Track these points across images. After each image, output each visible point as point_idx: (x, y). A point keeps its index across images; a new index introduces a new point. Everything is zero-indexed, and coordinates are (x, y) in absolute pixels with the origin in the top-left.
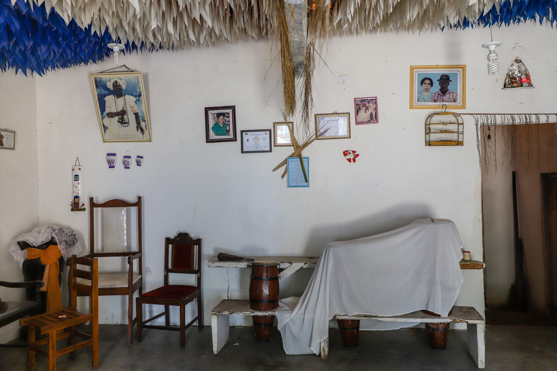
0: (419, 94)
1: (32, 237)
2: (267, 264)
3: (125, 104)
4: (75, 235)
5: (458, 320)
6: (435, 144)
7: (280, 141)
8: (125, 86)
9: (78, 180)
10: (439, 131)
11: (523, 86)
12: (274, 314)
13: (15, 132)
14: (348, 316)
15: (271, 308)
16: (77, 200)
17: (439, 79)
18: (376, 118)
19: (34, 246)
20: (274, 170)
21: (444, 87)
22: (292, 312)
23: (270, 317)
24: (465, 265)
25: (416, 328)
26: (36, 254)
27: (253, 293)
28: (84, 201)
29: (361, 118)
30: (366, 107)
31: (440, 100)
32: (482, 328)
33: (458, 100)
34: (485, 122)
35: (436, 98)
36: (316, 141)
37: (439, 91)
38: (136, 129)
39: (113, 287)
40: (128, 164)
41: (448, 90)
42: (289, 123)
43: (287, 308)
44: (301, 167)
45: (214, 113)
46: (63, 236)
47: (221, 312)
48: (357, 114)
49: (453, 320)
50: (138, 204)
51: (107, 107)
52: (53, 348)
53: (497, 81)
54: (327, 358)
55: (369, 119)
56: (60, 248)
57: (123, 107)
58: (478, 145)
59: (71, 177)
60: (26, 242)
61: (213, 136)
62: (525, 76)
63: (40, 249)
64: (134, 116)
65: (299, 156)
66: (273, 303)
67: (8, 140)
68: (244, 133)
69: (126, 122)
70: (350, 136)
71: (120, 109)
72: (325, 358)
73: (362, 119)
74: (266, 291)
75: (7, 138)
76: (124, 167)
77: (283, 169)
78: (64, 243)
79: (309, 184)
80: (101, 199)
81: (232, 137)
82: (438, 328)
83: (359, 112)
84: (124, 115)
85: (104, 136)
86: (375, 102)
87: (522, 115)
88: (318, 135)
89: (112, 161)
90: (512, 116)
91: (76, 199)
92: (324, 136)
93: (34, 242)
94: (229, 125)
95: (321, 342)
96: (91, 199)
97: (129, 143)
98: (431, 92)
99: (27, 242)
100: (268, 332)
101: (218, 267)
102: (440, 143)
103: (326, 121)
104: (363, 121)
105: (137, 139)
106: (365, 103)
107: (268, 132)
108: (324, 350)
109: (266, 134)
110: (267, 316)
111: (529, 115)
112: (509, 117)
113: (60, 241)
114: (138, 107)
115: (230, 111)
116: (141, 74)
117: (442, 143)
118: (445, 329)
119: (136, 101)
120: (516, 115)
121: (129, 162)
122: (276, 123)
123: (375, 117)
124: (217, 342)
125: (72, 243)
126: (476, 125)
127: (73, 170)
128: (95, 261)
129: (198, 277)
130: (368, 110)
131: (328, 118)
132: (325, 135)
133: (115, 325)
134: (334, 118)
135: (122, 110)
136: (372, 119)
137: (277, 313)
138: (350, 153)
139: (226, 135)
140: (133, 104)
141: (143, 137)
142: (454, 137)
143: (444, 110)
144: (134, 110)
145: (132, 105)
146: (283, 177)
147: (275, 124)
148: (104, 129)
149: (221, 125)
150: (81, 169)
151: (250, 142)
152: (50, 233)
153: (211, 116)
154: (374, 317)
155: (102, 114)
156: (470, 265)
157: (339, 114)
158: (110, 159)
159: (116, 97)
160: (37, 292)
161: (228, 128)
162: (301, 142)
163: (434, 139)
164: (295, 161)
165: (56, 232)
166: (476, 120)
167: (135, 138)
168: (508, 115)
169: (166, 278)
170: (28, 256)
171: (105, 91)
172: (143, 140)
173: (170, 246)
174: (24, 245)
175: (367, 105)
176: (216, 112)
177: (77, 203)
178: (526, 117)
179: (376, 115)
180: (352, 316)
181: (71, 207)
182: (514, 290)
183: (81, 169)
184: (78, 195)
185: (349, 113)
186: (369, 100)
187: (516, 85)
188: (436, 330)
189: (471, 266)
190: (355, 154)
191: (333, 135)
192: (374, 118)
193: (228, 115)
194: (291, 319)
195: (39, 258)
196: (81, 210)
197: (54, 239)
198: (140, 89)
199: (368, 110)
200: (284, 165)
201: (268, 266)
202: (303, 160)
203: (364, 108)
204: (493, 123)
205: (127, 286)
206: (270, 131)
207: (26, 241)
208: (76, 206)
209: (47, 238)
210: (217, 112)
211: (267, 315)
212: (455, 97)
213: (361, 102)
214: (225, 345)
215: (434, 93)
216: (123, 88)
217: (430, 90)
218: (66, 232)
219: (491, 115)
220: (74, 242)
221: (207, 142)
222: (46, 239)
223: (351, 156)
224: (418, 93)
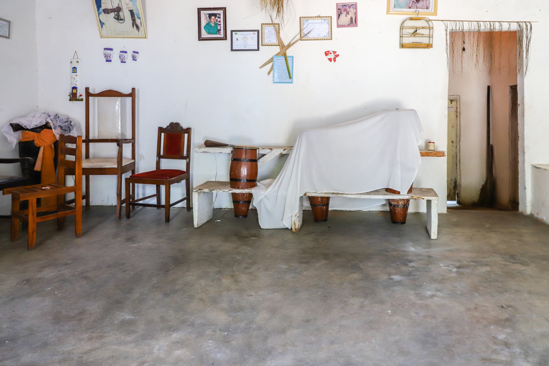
1: (27, 120)
2: (246, 147)
4: (71, 121)
5: (415, 196)
7: (266, 41)
9: (76, 72)
12: (251, 192)
14: (317, 193)
15: (249, 187)
16: (74, 91)
18: (355, 22)
19: (28, 129)
20: (261, 67)
22: (266, 190)
23: (248, 195)
24: (428, 153)
25: (386, 211)
26: (31, 136)
27: (233, 173)
28: (81, 92)
30: (347, 11)
31: (415, 7)
32: (435, 203)
33: (431, 7)
34: (454, 28)
35: (410, 5)
36: (300, 42)
38: (132, 25)
39: (103, 167)
40: (124, 58)
42: (276, 24)
43: (264, 187)
44: (286, 65)
45: (206, 14)
46: (58, 121)
47: (202, 189)
48: (339, 18)
49: (411, 197)
50: (132, 94)
51: (103, 3)
52: (33, 214)
54: (298, 231)
55: (350, 23)
56: (55, 132)
57: (119, 4)
58: (447, 49)
59: (70, 70)
60: (19, 124)
61: (204, 34)
63: (34, 132)
64: (129, 13)
65: (284, 55)
66: (252, 181)
68: (234, 33)
69: (122, 19)
70: (332, 38)
71: (115, 6)
72: (295, 231)
74: (244, 171)
76: (120, 61)
77: (269, 66)
78: (59, 129)
79: (292, 81)
80: (96, 89)
82: (398, 204)
83: (341, 16)
84: (120, 11)
85: (101, 32)
87: (487, 22)
88: (302, 35)
89: (109, 55)
92: (308, 37)
94: (220, 25)
95: (293, 216)
96: (87, 89)
97: (126, 39)
99: (21, 124)
100: (246, 209)
101: (204, 152)
104: (344, 24)
106: (346, 8)
107: (256, 33)
108: (295, 223)
109: (254, 34)
110: (244, 193)
111: (494, 22)
112: (475, 23)
113: (55, 126)
115: (221, 12)
118: (404, 206)
123: (355, 21)
124: (197, 217)
125: (67, 129)
126: (446, 30)
127: (71, 62)
128: (79, 138)
129: (187, 162)
131: (312, 20)
132: (309, 36)
133: (110, 206)
135: (117, 7)
137: (253, 191)
138: (330, 53)
139: (217, 34)
141: (138, 33)
142: (425, 41)
143: (417, 16)
144: (129, 7)
145: (127, 2)
146: (269, 73)
147: (262, 24)
148: (101, 25)
149: (213, 25)
150: (78, 62)
151: (240, 41)
152: (45, 118)
153: (203, 16)
154: (341, 194)
155: (98, 10)
157: (322, 17)
160: (26, 167)
161: (219, 28)
162: (286, 43)
164: (280, 59)
165: (51, 118)
166: (446, 26)
168: (474, 22)
169: (158, 163)
170: (23, 138)
173: (163, 134)
174: (17, 127)
175: (348, 10)
176: (208, 13)
177: (74, 93)
178: (490, 24)
179: (355, 19)
180: (321, 193)
181: (69, 98)
182: (483, 189)
183: (78, 62)
185: (331, 17)
188: (397, 207)
189: (433, 154)
190: (335, 54)
191: (316, 36)
192: (354, 22)
193: (219, 16)
194: (265, 196)
195: (34, 141)
196: (79, 100)
197: (48, 123)
200: (270, 63)
201: (247, 149)
202: (288, 58)
203: (345, 13)
204: (461, 29)
205: (116, 166)
206: (258, 31)
208: (73, 97)
209: (41, 122)
210: (209, 13)
211: (244, 192)
212: (428, 4)
213: (343, 7)
214: (207, 222)
218: (61, 119)
220: (70, 129)
221: (199, 40)
222: (40, 123)
223: (332, 56)
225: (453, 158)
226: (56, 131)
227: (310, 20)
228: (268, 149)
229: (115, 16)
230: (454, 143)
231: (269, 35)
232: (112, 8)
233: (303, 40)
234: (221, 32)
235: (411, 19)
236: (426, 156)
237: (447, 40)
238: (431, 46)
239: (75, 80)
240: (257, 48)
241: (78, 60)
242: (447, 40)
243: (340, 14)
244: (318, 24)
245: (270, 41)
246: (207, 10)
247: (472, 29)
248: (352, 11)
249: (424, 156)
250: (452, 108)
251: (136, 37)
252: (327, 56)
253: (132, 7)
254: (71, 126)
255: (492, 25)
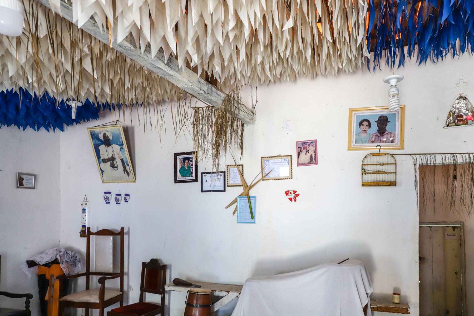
0: (357, 135)
3: (113, 152)
6: (367, 184)
7: (231, 182)
8: (112, 137)
9: (85, 213)
10: (371, 172)
11: (468, 124)
13: (35, 175)
17: (377, 120)
18: (315, 160)
20: (227, 208)
21: (382, 128)
29: (302, 160)
30: (306, 149)
31: (378, 141)
33: (396, 140)
34: (424, 162)
35: (373, 140)
36: (262, 182)
37: (377, 132)
40: (118, 200)
41: (386, 130)
42: (240, 165)
45: (181, 158)
48: (299, 157)
51: (102, 154)
53: (438, 119)
55: (309, 161)
56: (62, 267)
57: (112, 154)
58: (416, 186)
59: (81, 211)
61: (180, 178)
62: (472, 113)
65: (247, 195)
67: (28, 181)
68: (203, 175)
70: (292, 177)
73: (303, 161)
75: (27, 180)
81: (194, 178)
86: (314, 145)
87: (465, 154)
88: (264, 176)
89: (107, 198)
90: (454, 156)
91: (84, 230)
92: (269, 177)
93: (39, 261)
94: (192, 168)
98: (369, 133)
99: (35, 261)
102: (373, 183)
103: (271, 163)
104: (304, 163)
105: (125, 180)
106: (306, 146)
107: (223, 174)
114: (122, 154)
116: (121, 126)
117: (374, 184)
119: (120, 149)
120: (459, 154)
121: (118, 199)
122: (228, 166)
126: (415, 165)
130: (308, 153)
131: (273, 160)
134: (278, 160)
135: (112, 157)
136: (311, 161)
138: (291, 193)
139: (190, 177)
140: (119, 151)
141: (129, 178)
144: (120, 157)
146: (234, 213)
149: (186, 168)
150: (87, 204)
155: (99, 160)
156: (394, 308)
157: (282, 156)
158: (106, 196)
159: (106, 146)
161: (191, 171)
163: (388, 179)
164: (244, 200)
167: (123, 180)
168: (449, 155)
169: (142, 296)
171: (98, 141)
172: (129, 181)
174: (31, 264)
175: (308, 148)
178: (469, 156)
179: (315, 156)
183: (87, 204)
184: (85, 225)
185: (291, 156)
186: (310, 143)
187: (461, 123)
189: (395, 310)
190: (296, 194)
192: (314, 160)
198: (122, 139)
199: (308, 153)
202: (251, 198)
203: (305, 151)
207: (34, 260)
209: (51, 259)
213: (302, 145)
215: (371, 134)
216: (110, 139)
217: (368, 132)
219: (431, 155)
220: (75, 263)
222: (50, 259)
223: (292, 196)
224: (356, 135)
225: (457, 291)
226: (63, 265)
227: (271, 160)
228: (225, 292)
229: (111, 165)
230: (458, 275)
231: (234, 178)
232: (108, 158)
233: (265, 180)
234: (193, 175)
235: (373, 155)
236: (385, 312)
237: (416, 176)
238: (395, 185)
239: (84, 220)
240: (223, 189)
241: (87, 202)
242: (416, 176)
243: (300, 152)
244: (279, 163)
245: (234, 182)
246: (182, 154)
247: (447, 163)
248: (312, 148)
249: (384, 311)
250: (455, 235)
251: (127, 181)
252: (288, 196)
253: (122, 156)
254: (76, 260)
255: (471, 157)
